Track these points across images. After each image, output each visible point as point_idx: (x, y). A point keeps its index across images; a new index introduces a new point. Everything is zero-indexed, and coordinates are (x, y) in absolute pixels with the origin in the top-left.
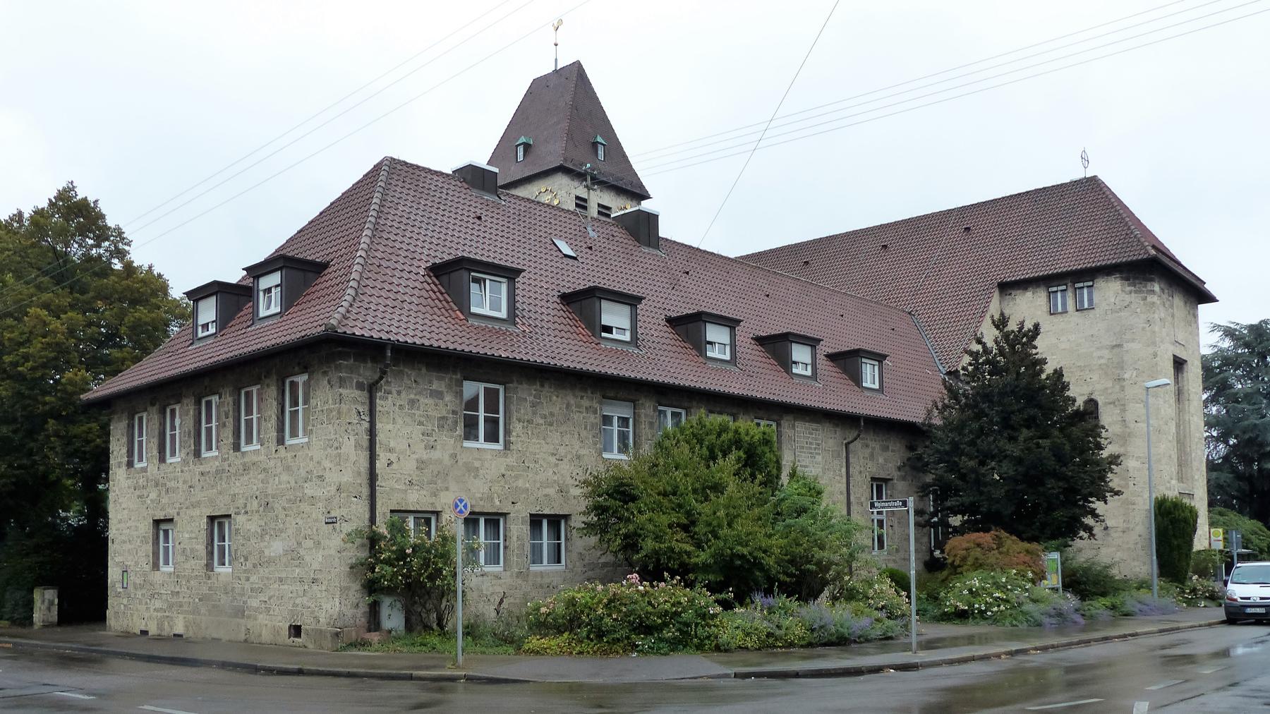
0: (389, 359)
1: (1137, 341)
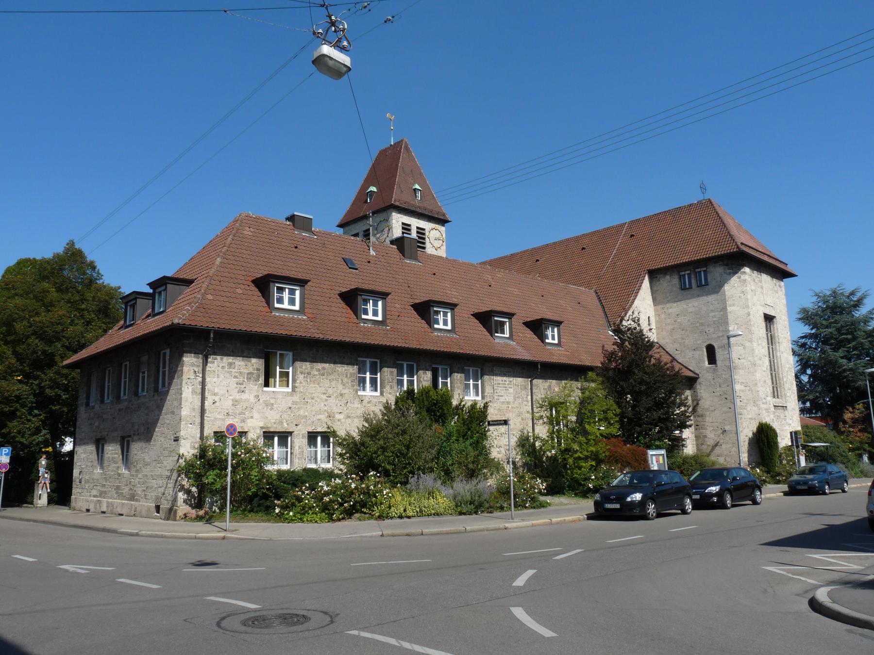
0: (212, 339)
1: (736, 305)
